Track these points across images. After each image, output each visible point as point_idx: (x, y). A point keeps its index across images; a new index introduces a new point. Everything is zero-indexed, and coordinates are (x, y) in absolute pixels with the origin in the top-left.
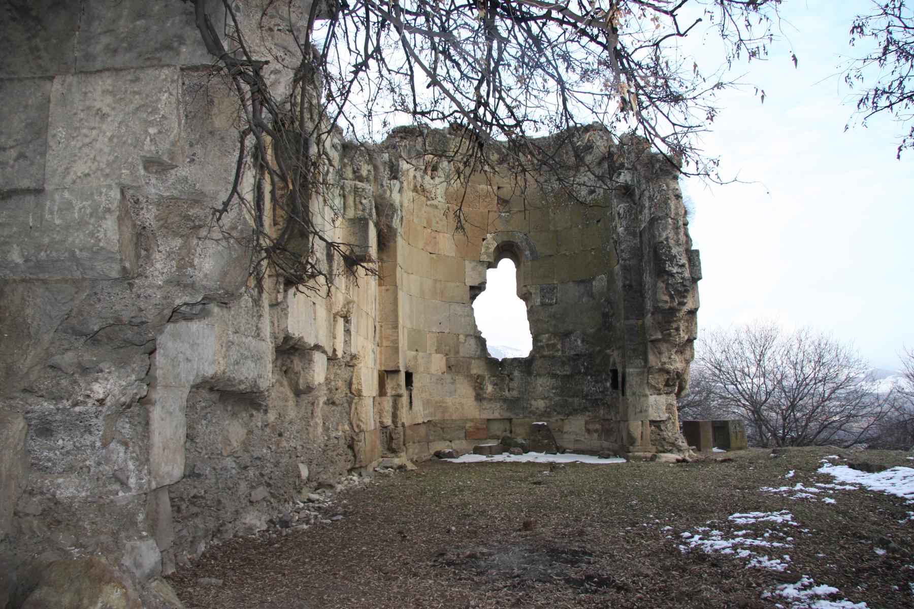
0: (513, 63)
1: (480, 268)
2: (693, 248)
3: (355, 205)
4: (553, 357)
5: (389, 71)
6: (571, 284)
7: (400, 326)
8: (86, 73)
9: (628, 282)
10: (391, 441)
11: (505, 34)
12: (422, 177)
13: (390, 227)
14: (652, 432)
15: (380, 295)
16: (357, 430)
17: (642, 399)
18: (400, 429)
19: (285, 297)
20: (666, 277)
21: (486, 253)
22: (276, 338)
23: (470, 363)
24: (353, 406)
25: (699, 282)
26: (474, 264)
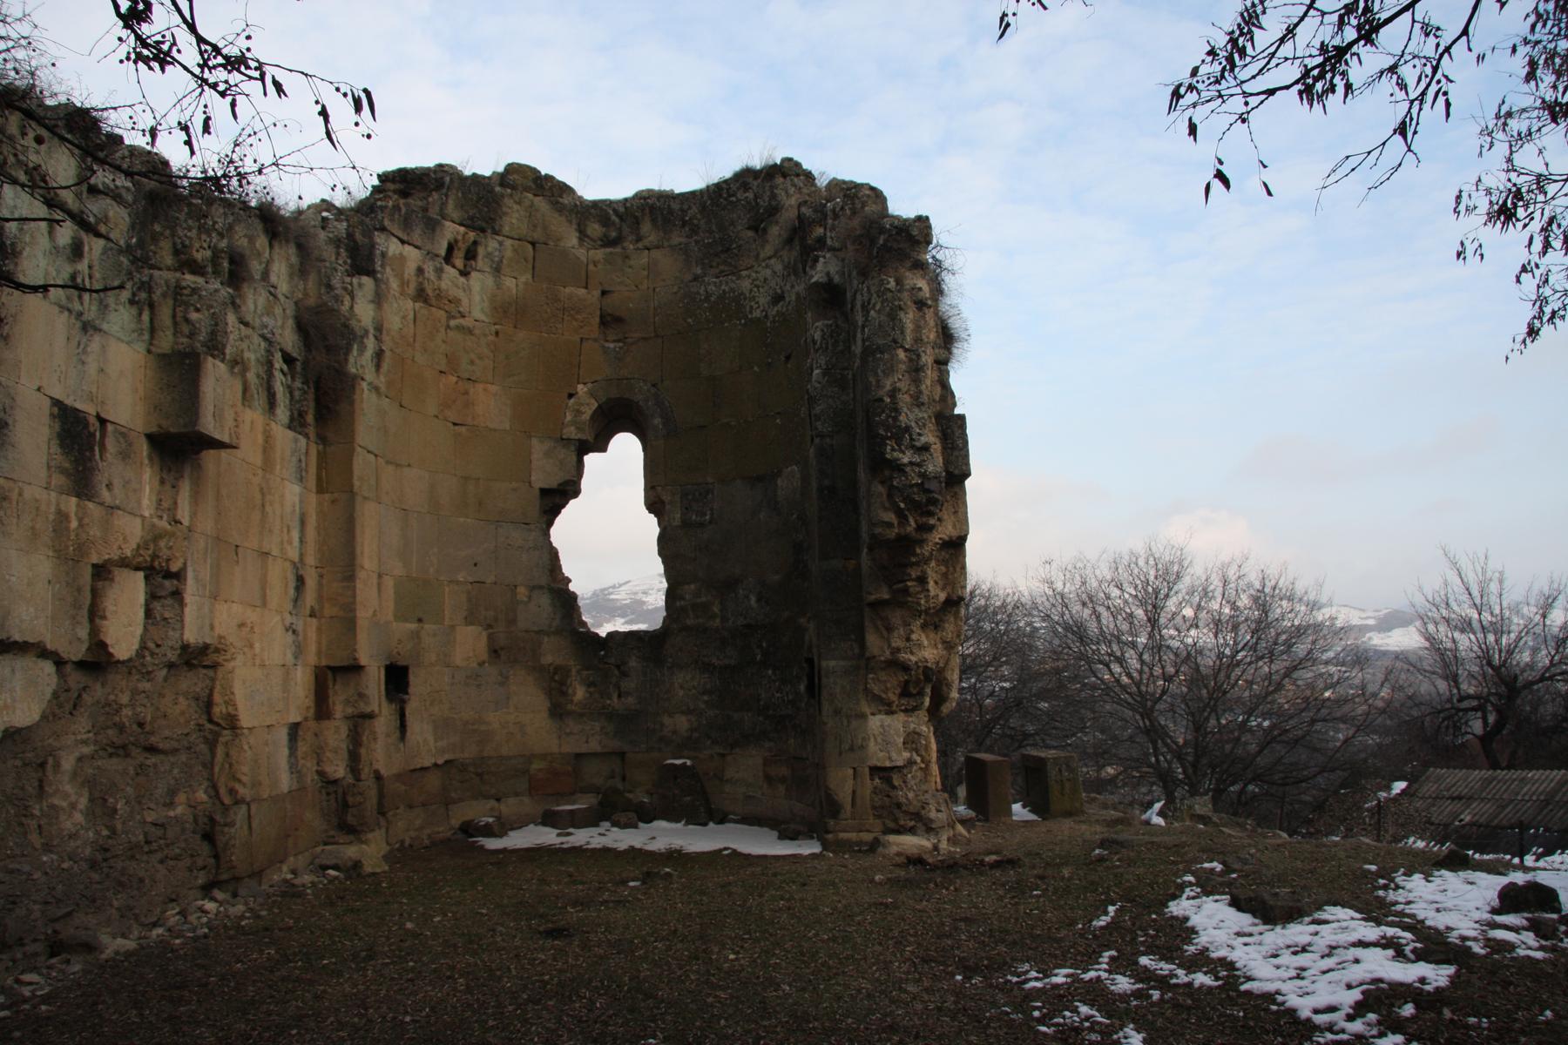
2: (957, 411)
3: (175, 324)
9: (826, 482)
10: (343, 809)
12: (439, 271)
14: (875, 791)
16: (227, 800)
17: (854, 723)
18: (368, 784)
20: (887, 473)
21: (574, 423)
24: (220, 751)
25: (968, 483)
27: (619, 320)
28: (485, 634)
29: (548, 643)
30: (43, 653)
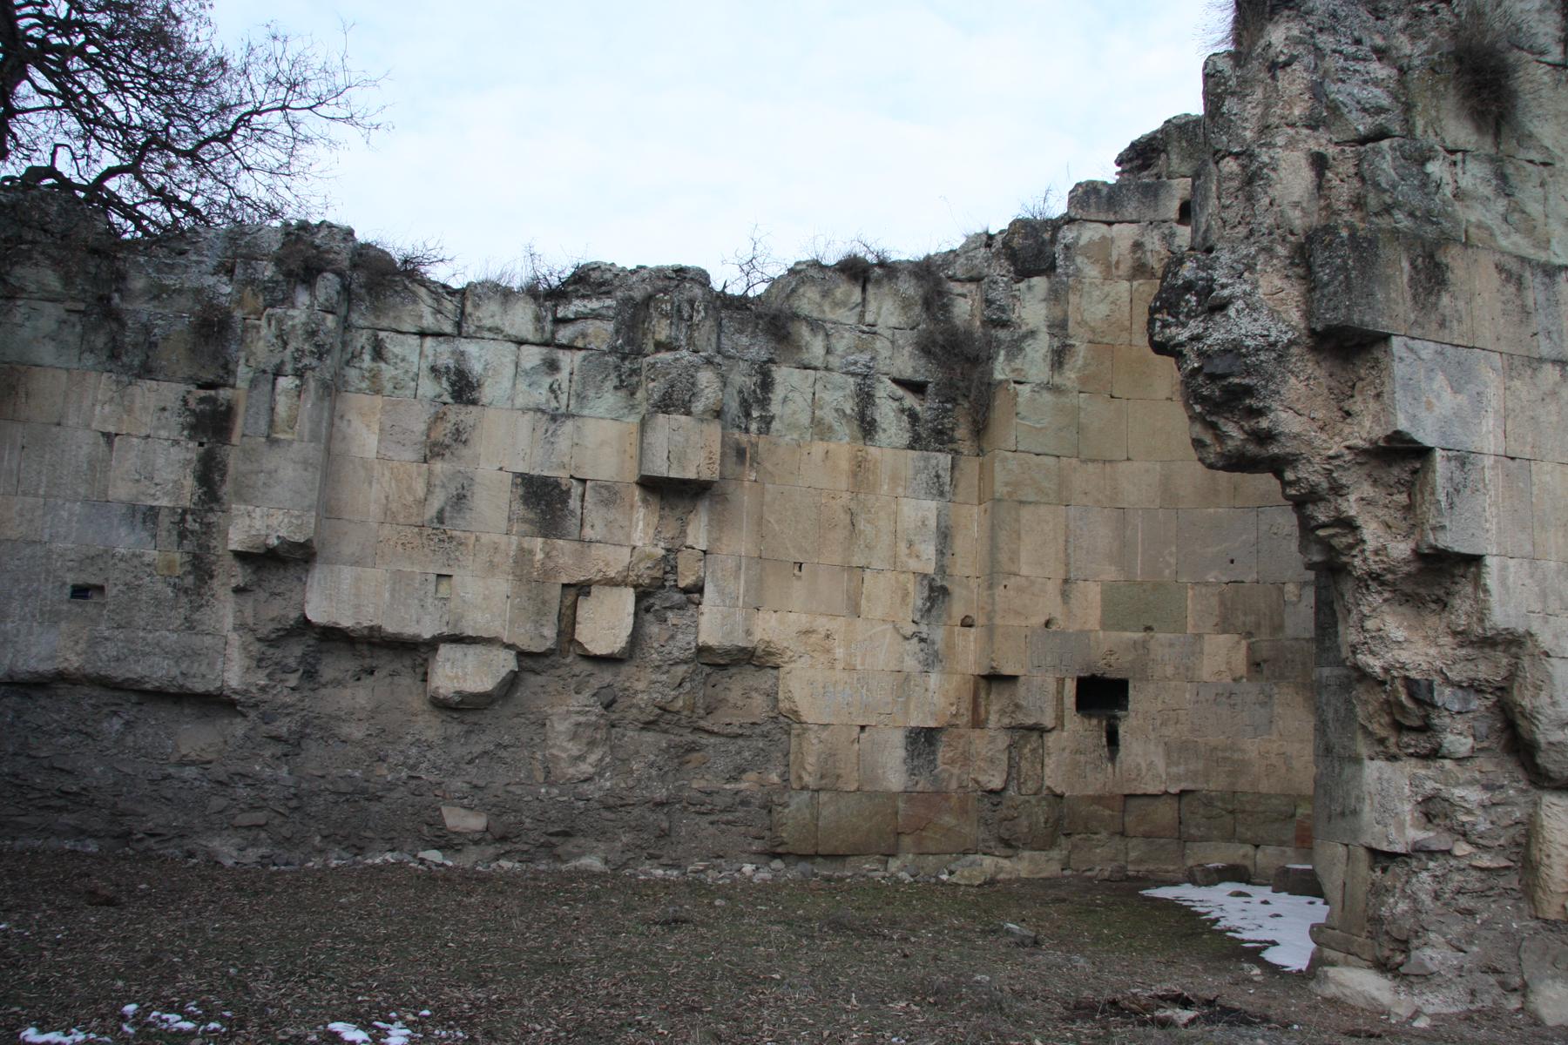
17: (1349, 770)
28: (1244, 643)
30: (509, 646)
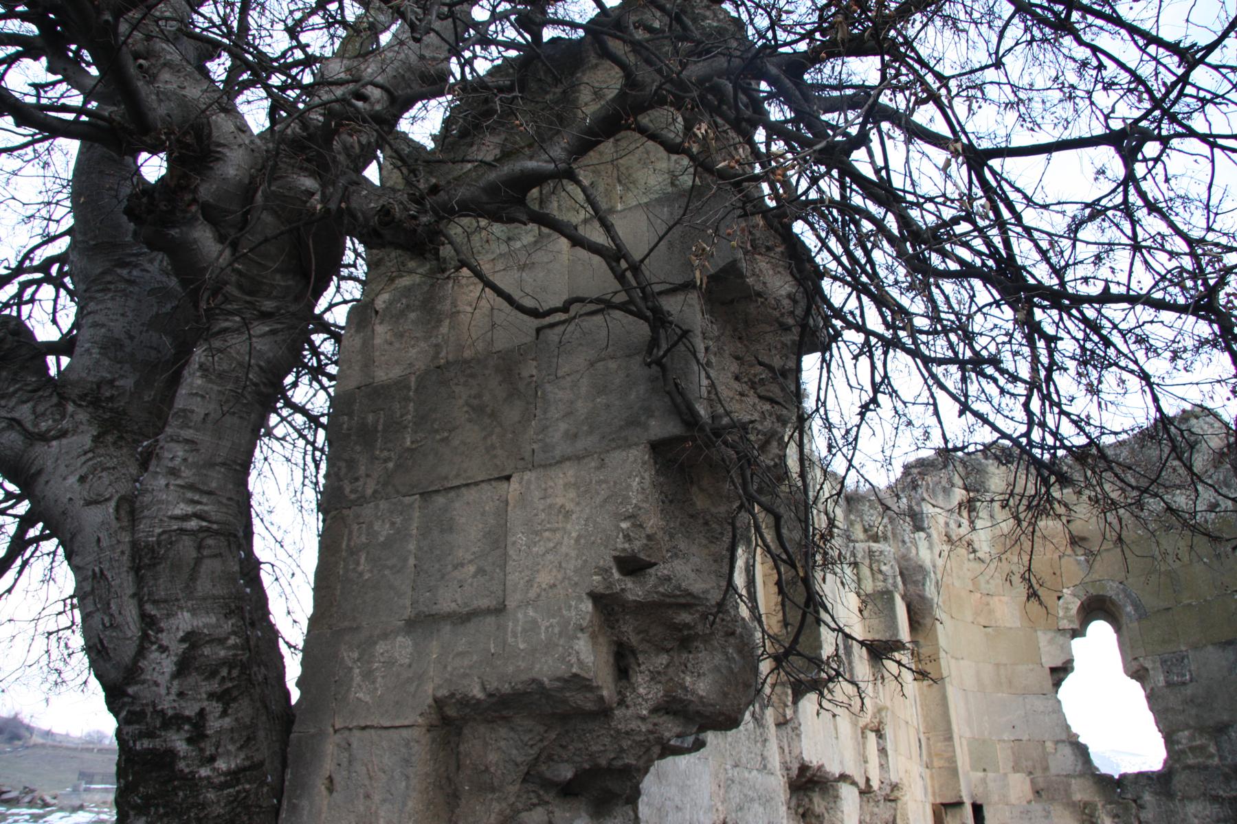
0: (1072, 365)
1: (1061, 639)
3: (873, 574)
4: (1206, 768)
5: (905, 403)
6: (1210, 648)
7: (956, 736)
8: (544, 466)
11: (1050, 330)
13: (922, 598)
15: (922, 694)
19: (795, 712)
22: (788, 769)
23: (1070, 785)
26: (1050, 635)
27: (1083, 539)
28: (1028, 779)
29: (1075, 784)
